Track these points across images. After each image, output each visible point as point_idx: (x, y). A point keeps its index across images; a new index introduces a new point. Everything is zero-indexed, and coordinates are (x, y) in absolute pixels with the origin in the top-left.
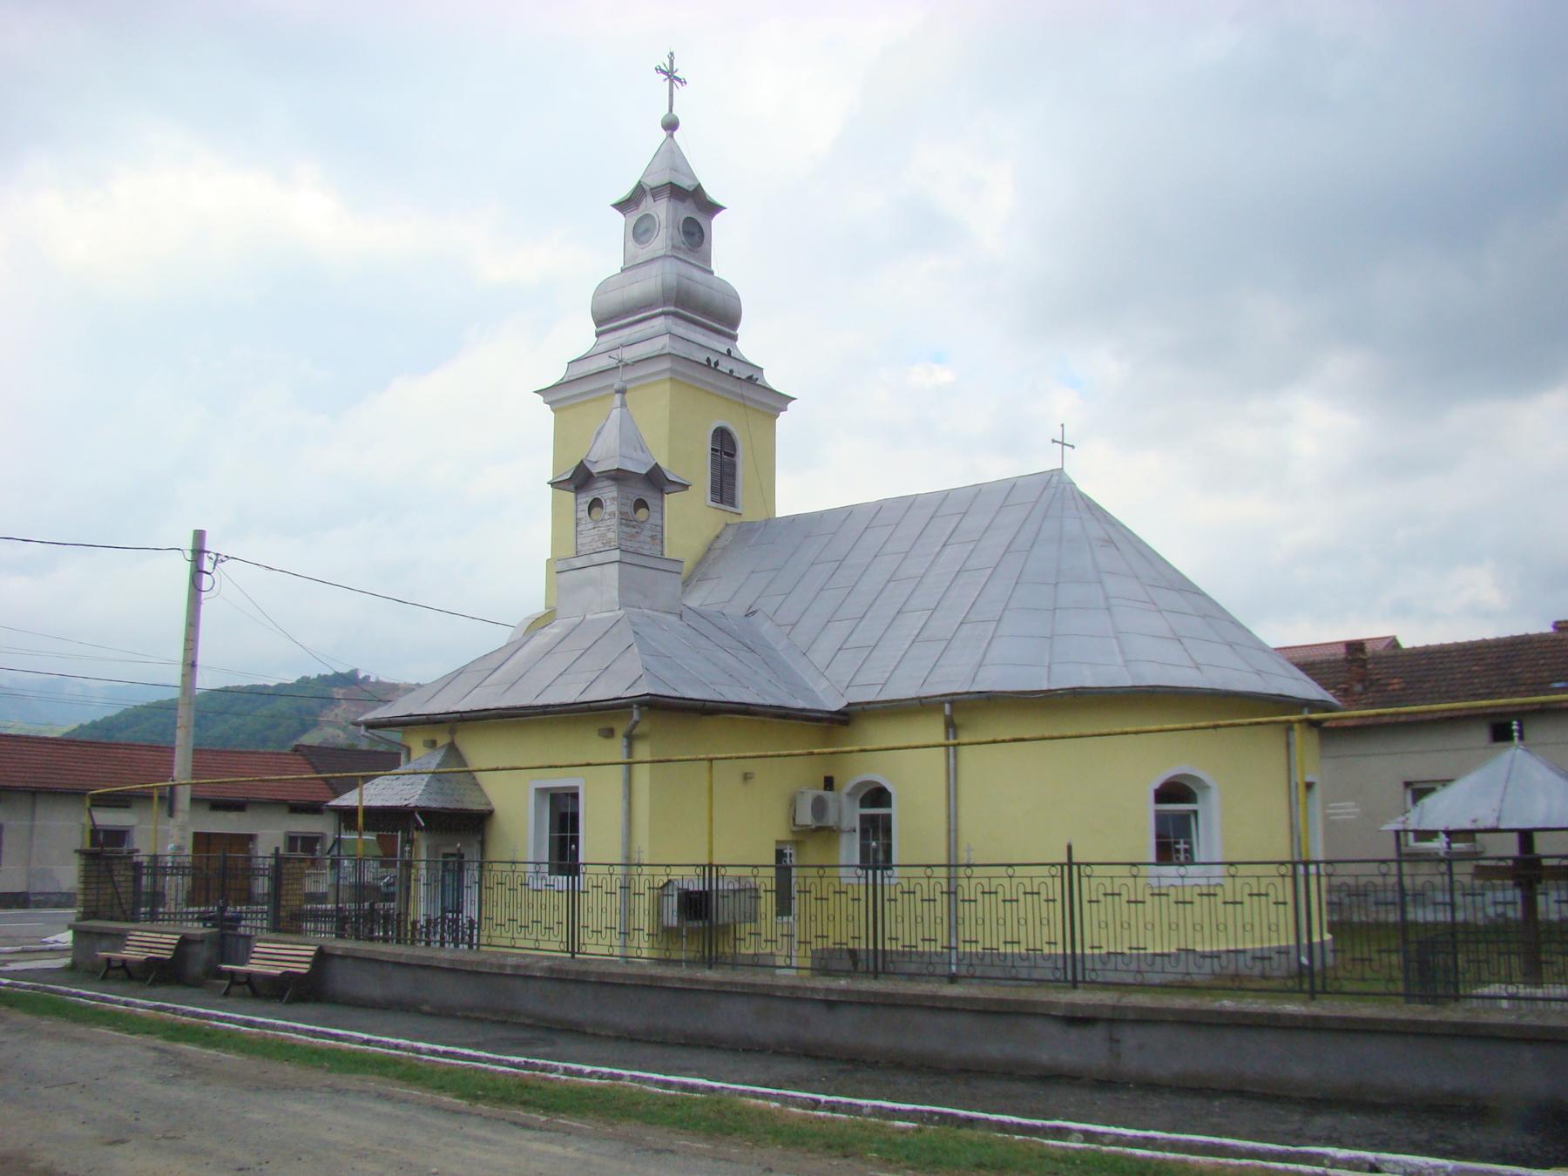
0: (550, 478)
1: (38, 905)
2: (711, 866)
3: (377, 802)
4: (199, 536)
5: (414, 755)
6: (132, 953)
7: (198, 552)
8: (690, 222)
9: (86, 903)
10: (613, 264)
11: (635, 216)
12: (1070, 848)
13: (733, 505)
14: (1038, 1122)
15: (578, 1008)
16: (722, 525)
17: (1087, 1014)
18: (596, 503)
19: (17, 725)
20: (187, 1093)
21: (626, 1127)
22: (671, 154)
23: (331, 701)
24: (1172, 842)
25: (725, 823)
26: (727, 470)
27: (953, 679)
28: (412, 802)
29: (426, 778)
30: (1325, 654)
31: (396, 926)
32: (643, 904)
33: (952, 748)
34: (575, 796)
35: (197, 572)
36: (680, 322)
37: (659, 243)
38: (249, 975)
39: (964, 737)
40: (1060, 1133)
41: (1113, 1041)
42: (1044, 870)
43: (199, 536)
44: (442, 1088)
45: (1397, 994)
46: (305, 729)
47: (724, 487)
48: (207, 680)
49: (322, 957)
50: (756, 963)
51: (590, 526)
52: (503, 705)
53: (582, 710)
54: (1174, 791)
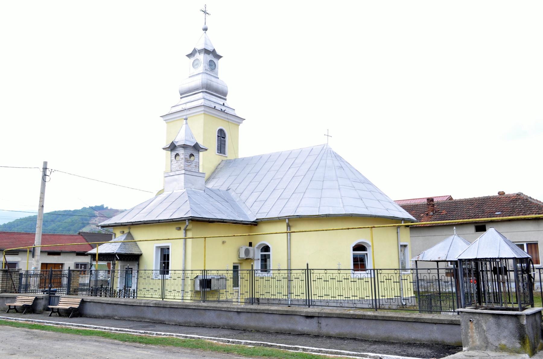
2: (205, 270)
3: (104, 252)
4: (45, 163)
5: (117, 236)
6: (18, 303)
7: (45, 169)
8: (211, 61)
11: (192, 59)
12: (308, 264)
13: (224, 154)
14: (290, 346)
15: (163, 316)
16: (221, 161)
18: (177, 155)
20: (35, 342)
21: (168, 347)
23: (95, 216)
24: (359, 263)
25: (217, 256)
26: (222, 142)
28: (115, 252)
29: (120, 243)
30: (417, 202)
31: (113, 294)
32: (189, 282)
33: (289, 233)
34: (168, 249)
35: (45, 175)
37: (201, 69)
40: (296, 349)
42: (300, 271)
43: (45, 163)
44: (116, 339)
46: (84, 226)
47: (221, 148)
49: (83, 302)
50: (227, 301)
52: (146, 220)
54: (359, 247)
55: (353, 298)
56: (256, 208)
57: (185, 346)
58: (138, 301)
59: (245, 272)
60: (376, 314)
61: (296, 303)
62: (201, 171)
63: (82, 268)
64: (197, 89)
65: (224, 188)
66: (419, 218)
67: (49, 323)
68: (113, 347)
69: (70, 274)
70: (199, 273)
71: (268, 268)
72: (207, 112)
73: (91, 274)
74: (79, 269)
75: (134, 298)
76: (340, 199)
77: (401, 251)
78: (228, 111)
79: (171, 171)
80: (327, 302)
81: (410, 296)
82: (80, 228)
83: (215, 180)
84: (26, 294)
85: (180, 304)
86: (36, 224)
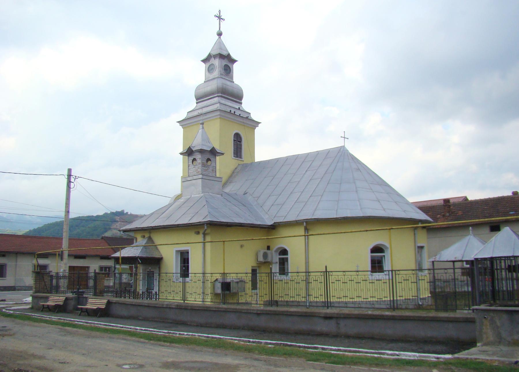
0: (181, 150)
1: (18, 290)
2: (224, 273)
3: (126, 255)
4: (70, 170)
6: (50, 303)
7: (69, 176)
9: (36, 288)
11: (208, 64)
12: (326, 267)
13: (241, 158)
14: (310, 346)
15: (185, 317)
17: (330, 316)
18: (194, 160)
19: (8, 230)
20: (68, 338)
21: (191, 346)
22: (220, 44)
23: (115, 221)
24: (377, 265)
25: (237, 260)
28: (137, 255)
29: (142, 247)
30: (434, 204)
31: (135, 295)
32: (209, 285)
33: (307, 236)
34: (188, 253)
35: (69, 182)
36: (223, 99)
37: (216, 73)
38: (87, 309)
39: (310, 233)
41: (338, 324)
43: (70, 170)
44: (141, 337)
45: (433, 309)
46: (106, 230)
47: (238, 152)
48: (73, 215)
49: (109, 303)
50: (247, 303)
51: (193, 167)
52: (165, 224)
53: (189, 226)
54: (377, 249)
55: (372, 299)
57: (207, 346)
58: (161, 303)
59: (264, 275)
60: (394, 313)
61: (315, 304)
62: (218, 175)
63: (106, 271)
66: (436, 220)
67: (79, 322)
68: (140, 344)
69: (95, 276)
70: (218, 276)
71: (286, 271)
72: (223, 116)
73: (115, 276)
74: (103, 272)
75: (156, 299)
77: (418, 252)
79: (189, 176)
80: (346, 303)
81: (426, 296)
82: (103, 233)
84: (57, 295)
85: (201, 305)
86: (62, 229)
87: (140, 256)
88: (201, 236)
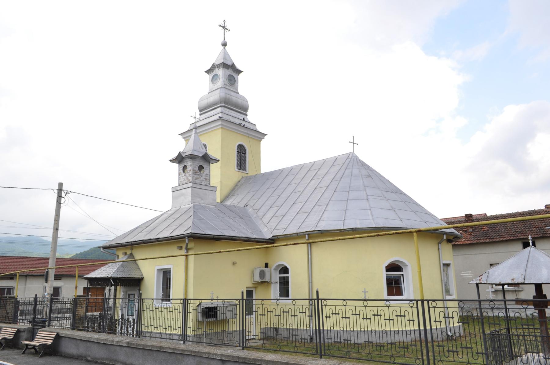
4: (61, 185)
5: (120, 257)
8: (230, 76)
10: (205, 91)
11: (212, 75)
13: (245, 170)
18: (185, 168)
24: (394, 286)
25: (222, 280)
26: (242, 158)
27: (310, 226)
28: (110, 276)
35: (60, 197)
37: (220, 83)
43: (61, 185)
47: (241, 164)
49: (58, 337)
51: (183, 175)
52: (145, 239)
54: (394, 267)
56: (273, 224)
64: (216, 104)
65: (242, 205)
76: (369, 211)
78: (247, 125)
83: (234, 197)
87: (113, 276)
88: (183, 252)
